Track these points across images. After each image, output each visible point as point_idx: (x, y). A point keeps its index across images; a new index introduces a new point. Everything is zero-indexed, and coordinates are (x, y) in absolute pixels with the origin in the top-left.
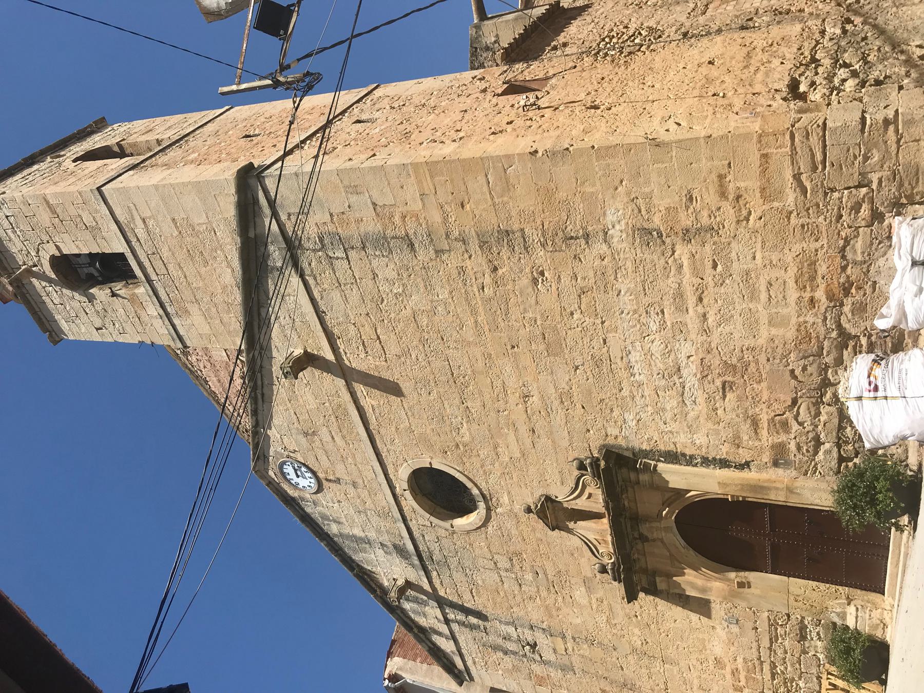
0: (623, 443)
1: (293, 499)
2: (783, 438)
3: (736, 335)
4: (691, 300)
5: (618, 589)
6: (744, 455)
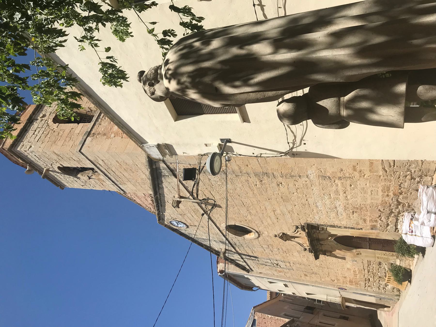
0: (314, 223)
1: (176, 229)
2: (375, 224)
3: (358, 201)
4: (341, 193)
5: (311, 256)
6: (359, 227)
